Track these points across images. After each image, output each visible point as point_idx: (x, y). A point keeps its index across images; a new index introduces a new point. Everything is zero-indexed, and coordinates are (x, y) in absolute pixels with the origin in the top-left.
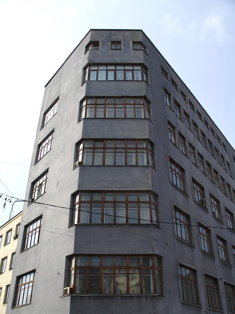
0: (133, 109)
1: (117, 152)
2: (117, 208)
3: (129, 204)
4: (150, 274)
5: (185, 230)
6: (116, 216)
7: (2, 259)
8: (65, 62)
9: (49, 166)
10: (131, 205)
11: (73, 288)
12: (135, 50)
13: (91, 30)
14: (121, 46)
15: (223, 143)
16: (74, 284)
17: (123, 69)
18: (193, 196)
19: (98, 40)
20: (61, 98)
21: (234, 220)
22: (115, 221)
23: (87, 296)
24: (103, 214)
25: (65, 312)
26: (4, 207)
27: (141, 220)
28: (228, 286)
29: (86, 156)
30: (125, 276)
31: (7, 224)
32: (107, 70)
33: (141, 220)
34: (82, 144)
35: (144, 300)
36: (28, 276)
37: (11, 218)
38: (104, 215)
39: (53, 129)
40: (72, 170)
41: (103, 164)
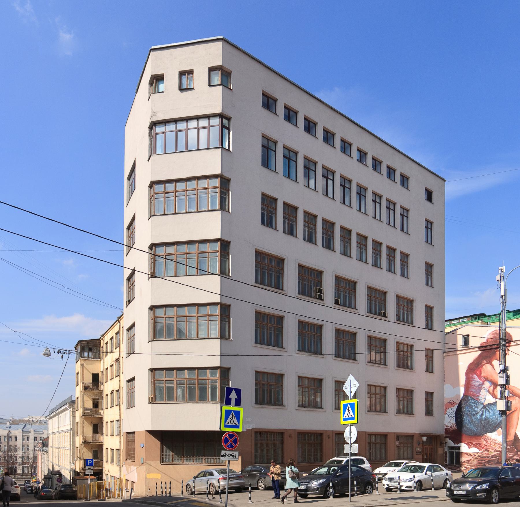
0: (406, 350)
1: (375, 391)
2: (119, 352)
3: (363, 491)
4: (265, 269)
5: (122, 319)
6: (356, 353)
7: (149, 308)
8: (70, 251)
9: (388, 472)
10: (67, 436)
11: (342, 398)
12: (334, 413)
13: (79, 342)
14: (83, 405)
15: (134, 219)
16: (456, 494)
17: (174, 129)
18: (167, 269)
19: (163, 73)
20: (171, 467)
21: (417, 432)
22: (371, 396)
23: (50, 499)
24: (59, 432)
25: (179, 324)
26: (62, 359)
27: (135, 271)
28: (223, 86)
29: (319, 352)
30: (71, 483)
31: (155, 144)
32: (199, 129)
33: (135, 271)
34: (307, 474)
35: (419, 449)
36: (365, 163)
37: (499, 359)
38: (125, 243)
39: (133, 322)
40: (341, 136)
41: (206, 494)
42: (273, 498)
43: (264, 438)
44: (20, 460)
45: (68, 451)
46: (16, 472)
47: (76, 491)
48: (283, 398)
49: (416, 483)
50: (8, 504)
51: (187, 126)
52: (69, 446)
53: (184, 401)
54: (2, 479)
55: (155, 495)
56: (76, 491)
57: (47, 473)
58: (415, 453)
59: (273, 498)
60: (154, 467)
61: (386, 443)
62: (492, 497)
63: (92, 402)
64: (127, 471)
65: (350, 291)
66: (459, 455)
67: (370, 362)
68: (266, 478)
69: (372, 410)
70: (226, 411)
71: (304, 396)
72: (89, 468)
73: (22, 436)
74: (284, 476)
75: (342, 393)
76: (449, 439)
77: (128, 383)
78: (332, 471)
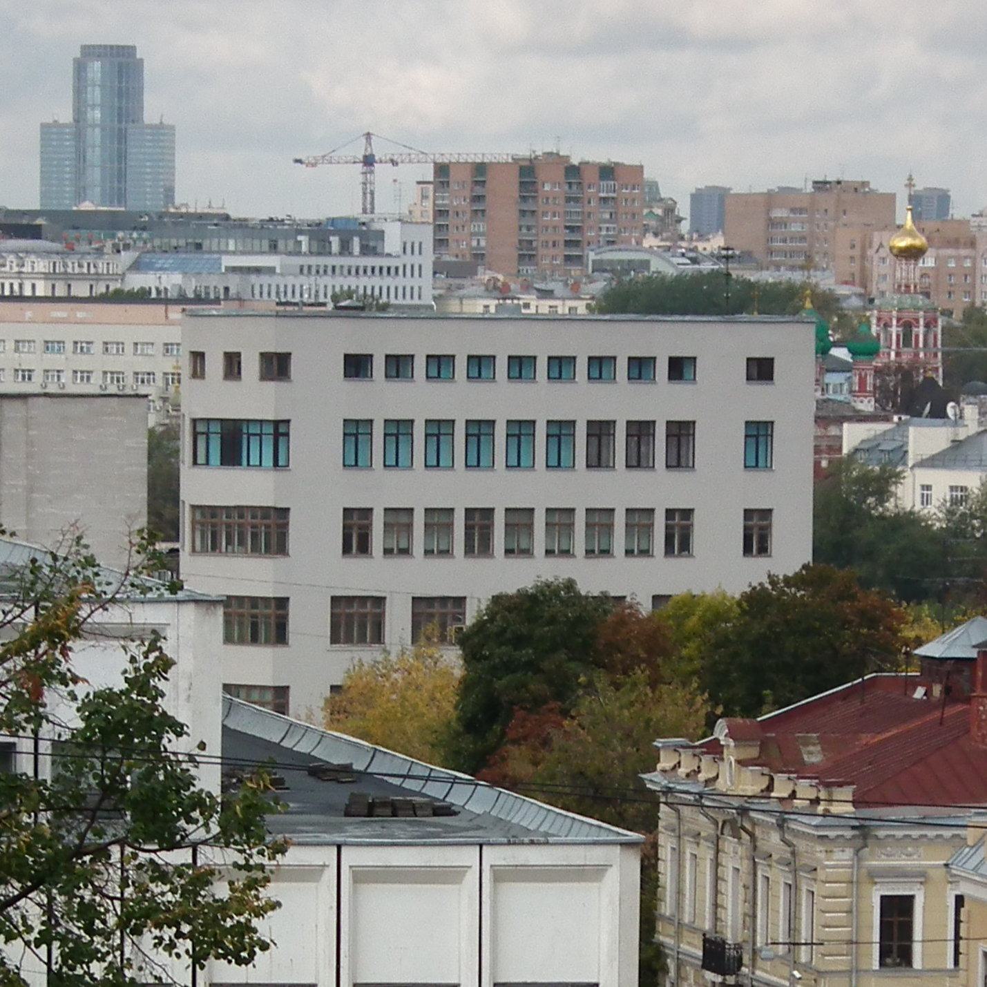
42: (162, 116)
43: (923, 495)
44: (770, 587)
45: (143, 621)
46: (948, 209)
47: (785, 576)
48: (642, 880)
49: (652, 800)
50: (128, 774)
51: (670, 920)
52: (148, 622)
53: (267, 642)
54: (585, 185)
55: (18, 750)
56: (785, 576)
57: (667, 951)
58: (203, 753)
59: (162, 116)
60: (778, 944)
61: (330, 253)
62: (91, 697)
63: (528, 154)
64: (270, 913)
65: (118, 953)
66: (26, 523)
67: (123, 343)
68: (681, 215)
69: (557, 361)
70: (910, 899)
71: (769, 963)
72: (129, 959)
73: (24, 341)
74: (604, 520)
75: (21, 982)
76: (800, 190)
77: (529, 550)
78: (92, 763)
